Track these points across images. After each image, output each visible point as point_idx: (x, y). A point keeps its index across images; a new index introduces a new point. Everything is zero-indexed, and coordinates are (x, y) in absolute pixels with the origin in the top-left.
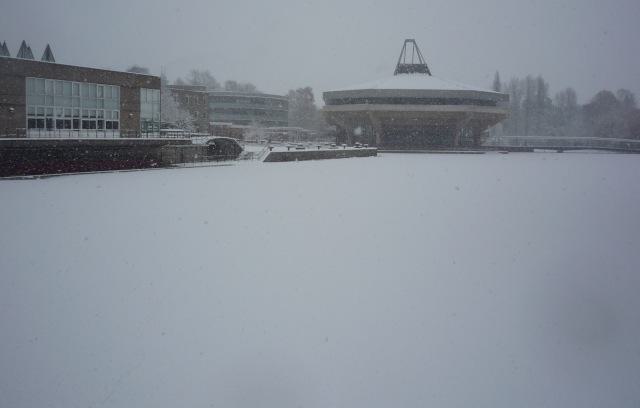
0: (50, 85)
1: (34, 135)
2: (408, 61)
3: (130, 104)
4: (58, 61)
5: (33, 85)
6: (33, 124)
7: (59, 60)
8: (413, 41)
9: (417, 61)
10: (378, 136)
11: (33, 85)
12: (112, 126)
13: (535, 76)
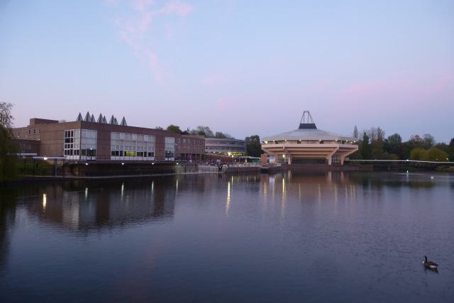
0: (122, 136)
1: (113, 158)
2: (306, 122)
3: (160, 144)
4: (128, 125)
5: (114, 136)
6: (116, 153)
7: (129, 124)
8: (309, 113)
9: (310, 122)
10: (93, 158)
11: (114, 136)
12: (150, 154)
13: (376, 127)
